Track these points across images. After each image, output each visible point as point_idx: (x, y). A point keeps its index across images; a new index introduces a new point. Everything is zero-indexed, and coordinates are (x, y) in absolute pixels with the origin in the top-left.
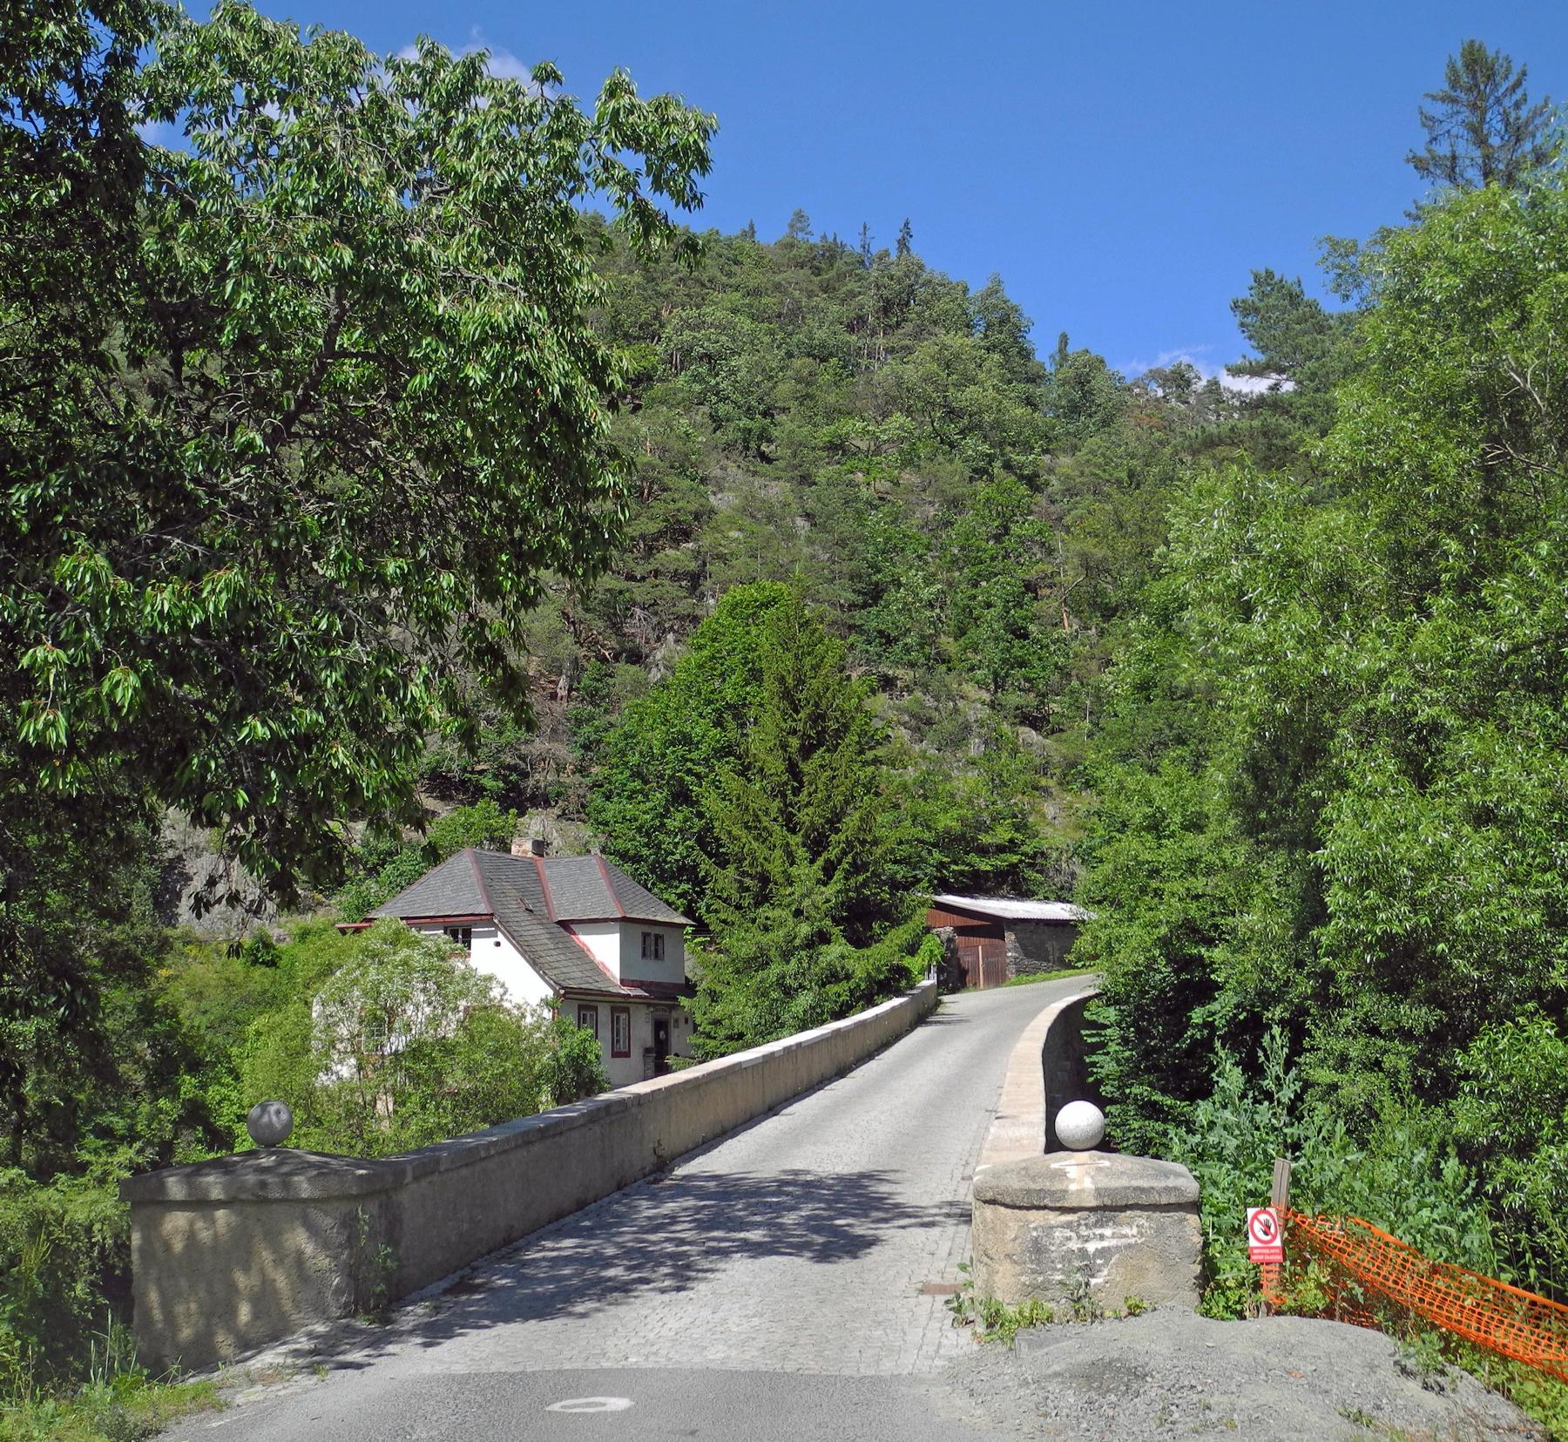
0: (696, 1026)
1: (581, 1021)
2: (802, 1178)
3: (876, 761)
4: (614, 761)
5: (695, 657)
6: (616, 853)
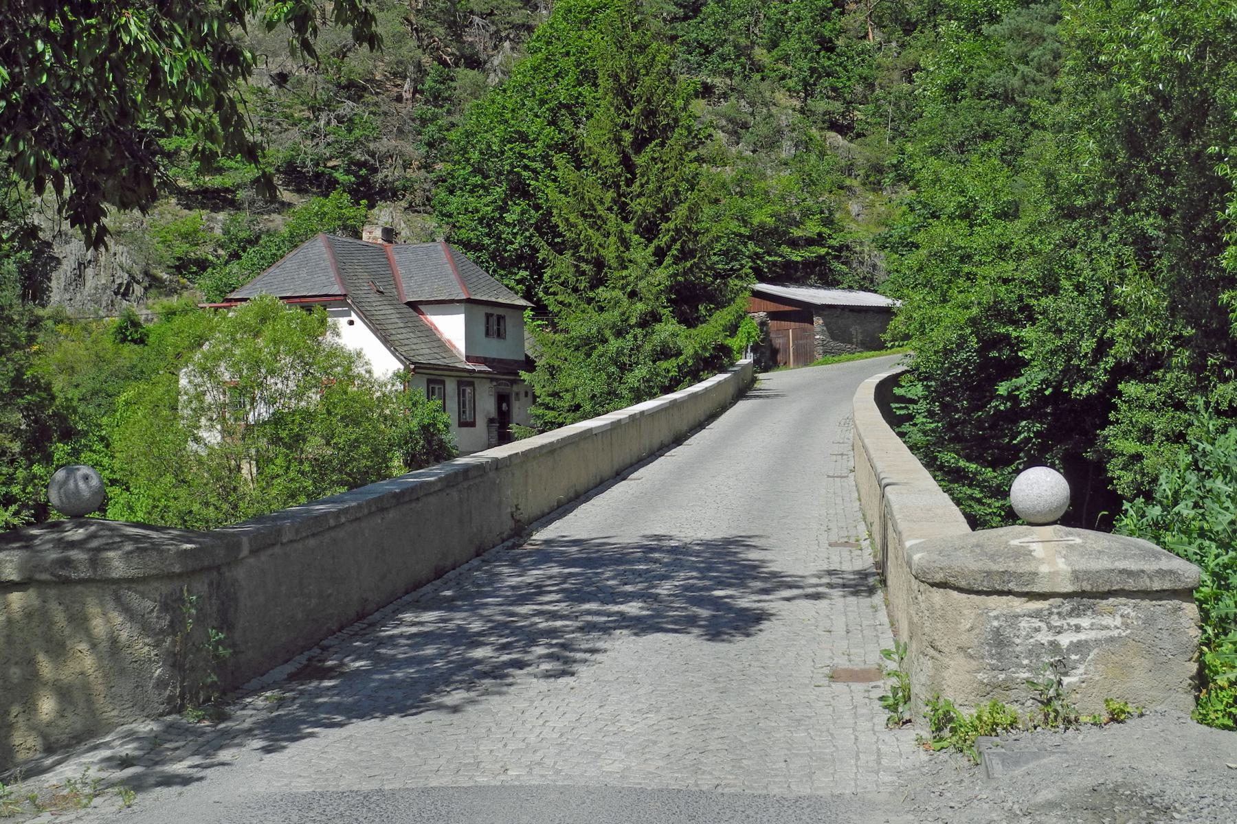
0: (535, 397)
1: (430, 394)
2: (666, 543)
3: (699, 160)
4: (456, 158)
5: (530, 61)
6: (459, 242)
